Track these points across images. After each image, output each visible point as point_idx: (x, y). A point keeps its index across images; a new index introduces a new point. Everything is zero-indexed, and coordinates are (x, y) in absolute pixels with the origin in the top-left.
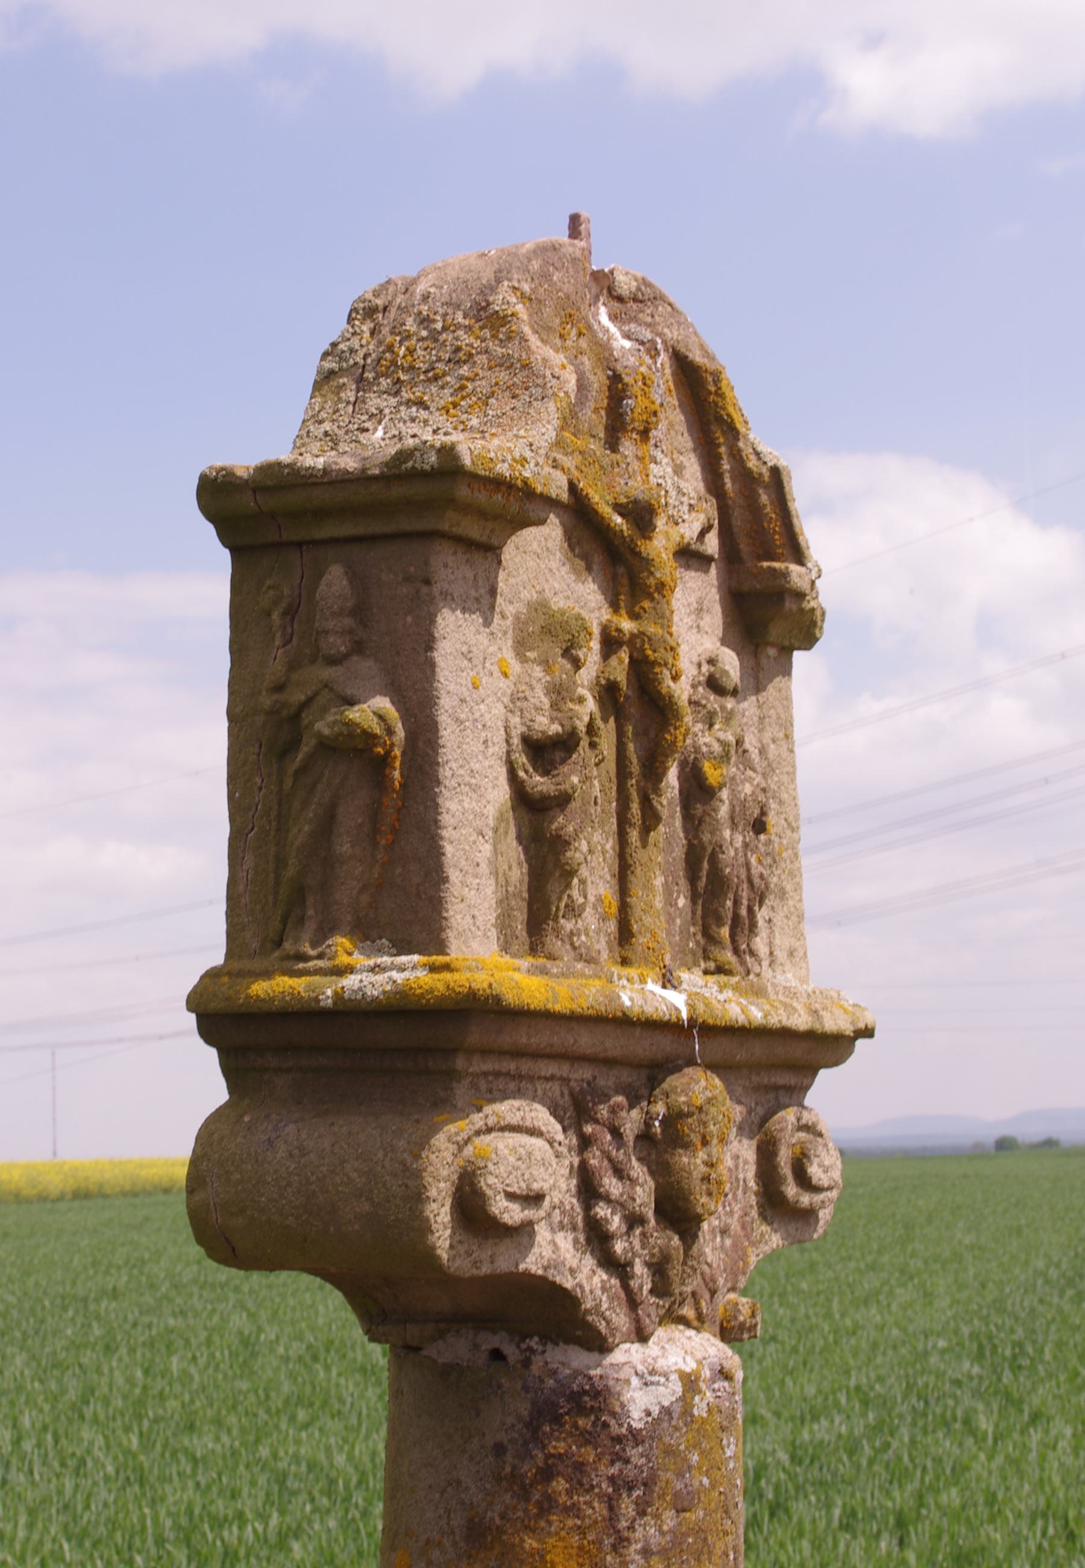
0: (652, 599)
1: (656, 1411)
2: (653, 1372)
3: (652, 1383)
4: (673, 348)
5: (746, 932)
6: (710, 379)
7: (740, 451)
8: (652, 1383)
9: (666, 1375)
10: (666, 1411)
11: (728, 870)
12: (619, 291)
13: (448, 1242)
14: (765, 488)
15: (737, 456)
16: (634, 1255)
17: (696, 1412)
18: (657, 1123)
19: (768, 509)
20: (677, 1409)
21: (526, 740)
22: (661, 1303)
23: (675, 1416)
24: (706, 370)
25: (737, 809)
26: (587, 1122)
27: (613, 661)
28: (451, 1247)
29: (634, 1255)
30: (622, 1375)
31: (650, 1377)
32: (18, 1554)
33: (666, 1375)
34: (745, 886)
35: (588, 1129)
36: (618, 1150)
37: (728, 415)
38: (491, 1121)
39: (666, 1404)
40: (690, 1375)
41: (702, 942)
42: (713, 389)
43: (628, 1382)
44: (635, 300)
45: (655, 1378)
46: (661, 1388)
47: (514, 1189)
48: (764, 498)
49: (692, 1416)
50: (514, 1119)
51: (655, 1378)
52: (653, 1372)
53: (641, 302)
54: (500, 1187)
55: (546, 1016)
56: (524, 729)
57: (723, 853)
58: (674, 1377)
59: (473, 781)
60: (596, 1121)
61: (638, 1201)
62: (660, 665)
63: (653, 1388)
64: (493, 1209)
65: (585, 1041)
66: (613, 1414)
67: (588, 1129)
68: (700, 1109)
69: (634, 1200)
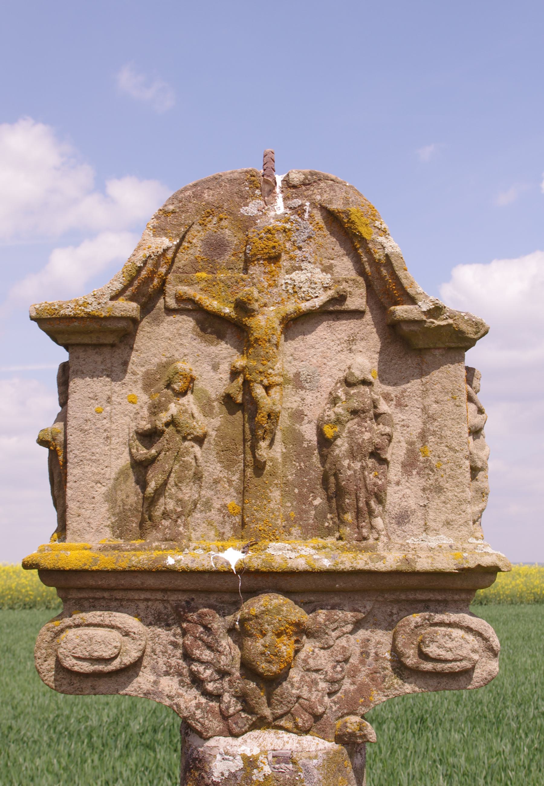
0: (254, 347)
1: (226, 774)
2: (227, 753)
3: (226, 759)
4: (320, 205)
5: (367, 516)
6: (343, 216)
7: (370, 249)
8: (226, 759)
9: (234, 756)
10: (233, 775)
11: (344, 483)
12: (293, 183)
13: (53, 678)
14: (384, 266)
15: (369, 252)
16: (225, 691)
17: (254, 778)
18: (237, 623)
19: (388, 278)
20: (240, 775)
21: (137, 433)
22: (250, 717)
23: (239, 778)
24: (339, 212)
25: (355, 448)
26: (184, 622)
27: (235, 384)
28: (55, 680)
29: (225, 691)
30: (213, 753)
31: (227, 755)
32: (358, 766)
33: (234, 756)
34: (363, 490)
35: (184, 625)
36: (208, 636)
37: (358, 232)
38: (76, 622)
39: (233, 771)
40: (249, 757)
41: (337, 522)
42: (346, 220)
43: (215, 756)
44: (305, 184)
45: (227, 757)
46: (231, 763)
47: (79, 655)
48: (384, 272)
49: (252, 780)
50: (97, 620)
51: (227, 757)
52: (227, 753)
53: (309, 184)
54: (67, 653)
55: (114, 572)
56: (135, 428)
57: (341, 474)
58: (238, 757)
59: (94, 458)
60: (189, 621)
61: (222, 663)
62: (252, 381)
63: (227, 761)
64: (65, 664)
65: (151, 582)
66: (206, 772)
67: (184, 625)
68: (256, 617)
69: (219, 662)
